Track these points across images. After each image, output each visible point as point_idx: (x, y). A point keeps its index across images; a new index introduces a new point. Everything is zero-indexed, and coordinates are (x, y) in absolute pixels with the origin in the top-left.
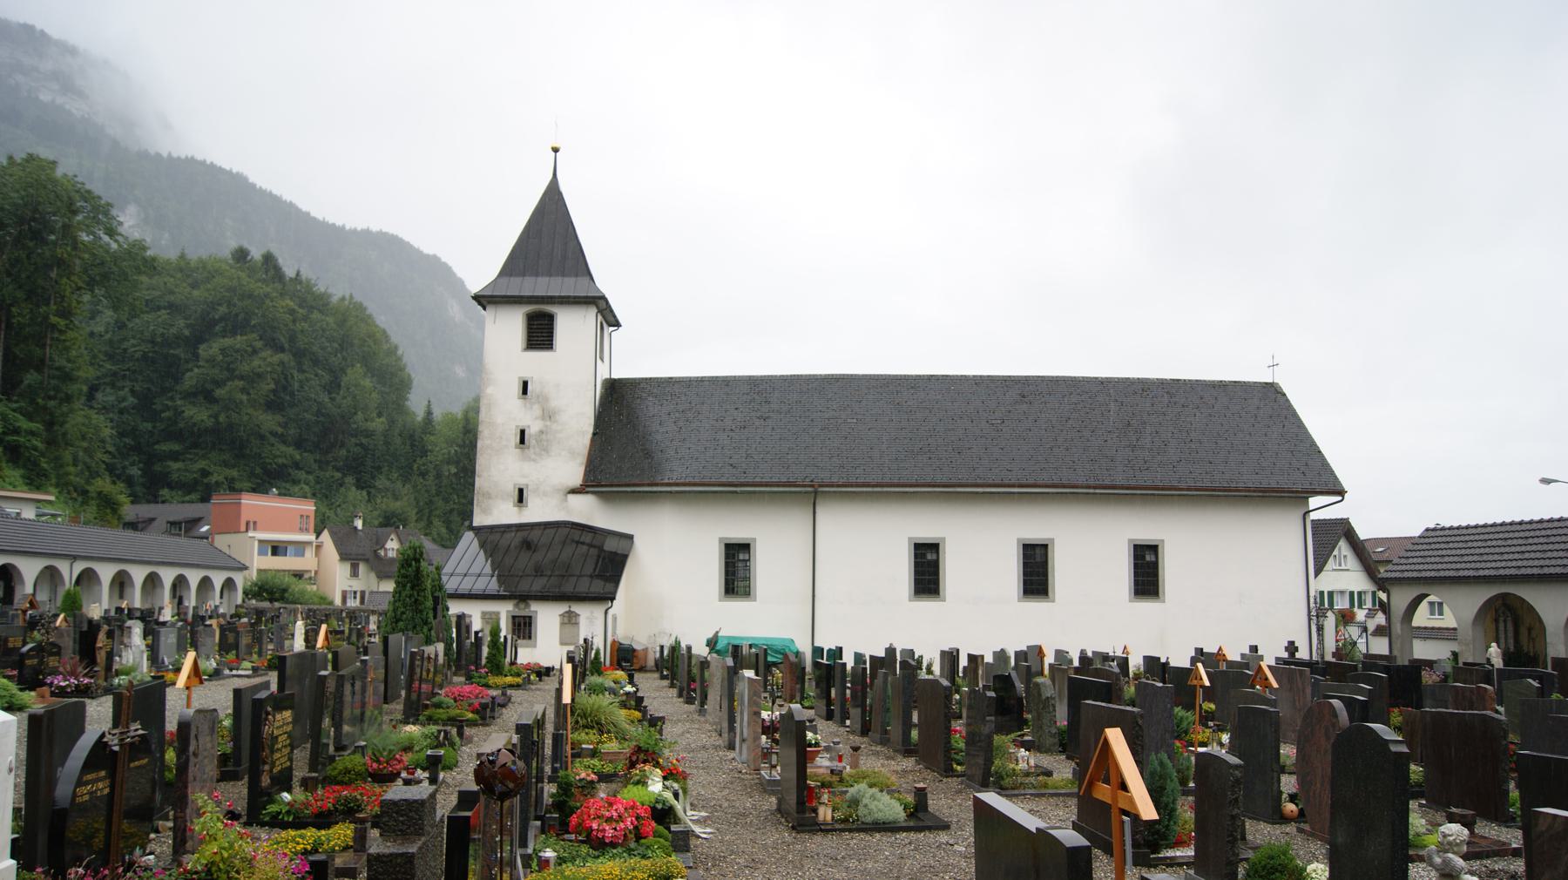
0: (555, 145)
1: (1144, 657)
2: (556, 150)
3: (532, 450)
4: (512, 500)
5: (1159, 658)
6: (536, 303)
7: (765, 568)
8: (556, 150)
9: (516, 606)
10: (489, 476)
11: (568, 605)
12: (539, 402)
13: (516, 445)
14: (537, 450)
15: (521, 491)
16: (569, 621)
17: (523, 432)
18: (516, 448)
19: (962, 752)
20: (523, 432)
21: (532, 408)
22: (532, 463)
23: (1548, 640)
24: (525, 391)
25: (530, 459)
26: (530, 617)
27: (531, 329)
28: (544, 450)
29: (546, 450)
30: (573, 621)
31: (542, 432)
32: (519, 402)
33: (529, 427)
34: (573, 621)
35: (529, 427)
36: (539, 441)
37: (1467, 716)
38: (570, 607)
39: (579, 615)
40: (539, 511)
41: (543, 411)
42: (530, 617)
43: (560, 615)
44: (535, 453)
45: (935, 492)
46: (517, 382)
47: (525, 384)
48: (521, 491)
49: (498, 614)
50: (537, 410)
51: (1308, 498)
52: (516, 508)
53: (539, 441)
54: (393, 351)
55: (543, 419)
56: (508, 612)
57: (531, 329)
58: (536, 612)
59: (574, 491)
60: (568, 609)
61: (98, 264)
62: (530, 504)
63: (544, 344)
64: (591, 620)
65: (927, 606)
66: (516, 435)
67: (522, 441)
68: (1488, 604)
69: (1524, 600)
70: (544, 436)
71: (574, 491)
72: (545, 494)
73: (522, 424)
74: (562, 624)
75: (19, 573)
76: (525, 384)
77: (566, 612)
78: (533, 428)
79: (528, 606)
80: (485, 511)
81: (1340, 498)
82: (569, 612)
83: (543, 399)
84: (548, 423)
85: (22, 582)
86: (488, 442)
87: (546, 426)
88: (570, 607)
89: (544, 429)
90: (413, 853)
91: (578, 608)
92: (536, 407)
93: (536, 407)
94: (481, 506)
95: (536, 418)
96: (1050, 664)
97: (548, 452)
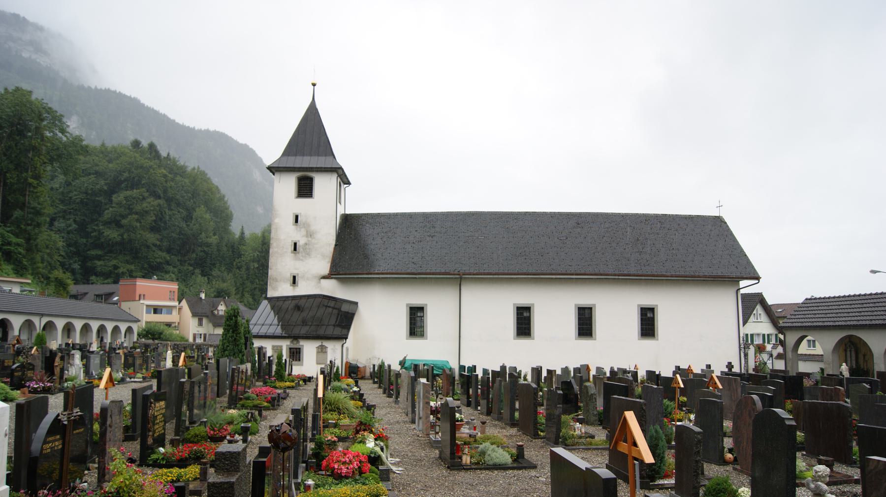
0: (313, 82)
1: (647, 371)
2: (314, 85)
3: (300, 254)
4: (289, 282)
5: (655, 372)
6: (303, 171)
7: (432, 321)
8: (314, 85)
9: (292, 342)
10: (276, 269)
11: (321, 342)
12: (305, 227)
13: (291, 251)
14: (304, 254)
15: (294, 277)
16: (322, 351)
17: (295, 244)
18: (292, 253)
19: (544, 424)
20: (295, 244)
21: (300, 230)
22: (301, 261)
23: (875, 362)
24: (297, 221)
25: (299, 259)
26: (300, 349)
27: (300, 186)
28: (307, 254)
29: (308, 254)
30: (324, 351)
31: (306, 244)
32: (293, 227)
33: (299, 241)
34: (324, 351)
35: (299, 241)
36: (305, 249)
37: (829, 405)
38: (322, 343)
39: (327, 347)
40: (304, 289)
41: (307, 232)
42: (300, 349)
43: (316, 348)
44: (302, 256)
45: (528, 278)
46: (292, 216)
47: (297, 217)
48: (294, 277)
49: (281, 347)
50: (303, 232)
51: (739, 281)
52: (292, 287)
53: (305, 249)
54: (222, 198)
55: (307, 237)
56: (287, 345)
57: (300, 186)
58: (303, 346)
59: (324, 277)
60: (321, 344)
61: (56, 149)
62: (299, 285)
63: (307, 194)
64: (334, 350)
65: (524, 342)
66: (292, 246)
67: (295, 249)
68: (841, 341)
69: (861, 339)
70: (307, 247)
71: (324, 277)
72: (308, 279)
73: (295, 240)
74: (318, 352)
75: (11, 324)
76: (297, 217)
77: (320, 346)
78: (301, 242)
79: (298, 342)
80: (274, 289)
81: (757, 281)
82: (322, 346)
83: (307, 226)
84: (310, 239)
85: (12, 329)
86: (276, 250)
87: (309, 241)
88: (322, 343)
89: (308, 242)
90: (233, 482)
91: (326, 344)
92: (303, 230)
93: (303, 230)
94: (272, 286)
95: (303, 236)
96: (593, 375)
97: (309, 255)
